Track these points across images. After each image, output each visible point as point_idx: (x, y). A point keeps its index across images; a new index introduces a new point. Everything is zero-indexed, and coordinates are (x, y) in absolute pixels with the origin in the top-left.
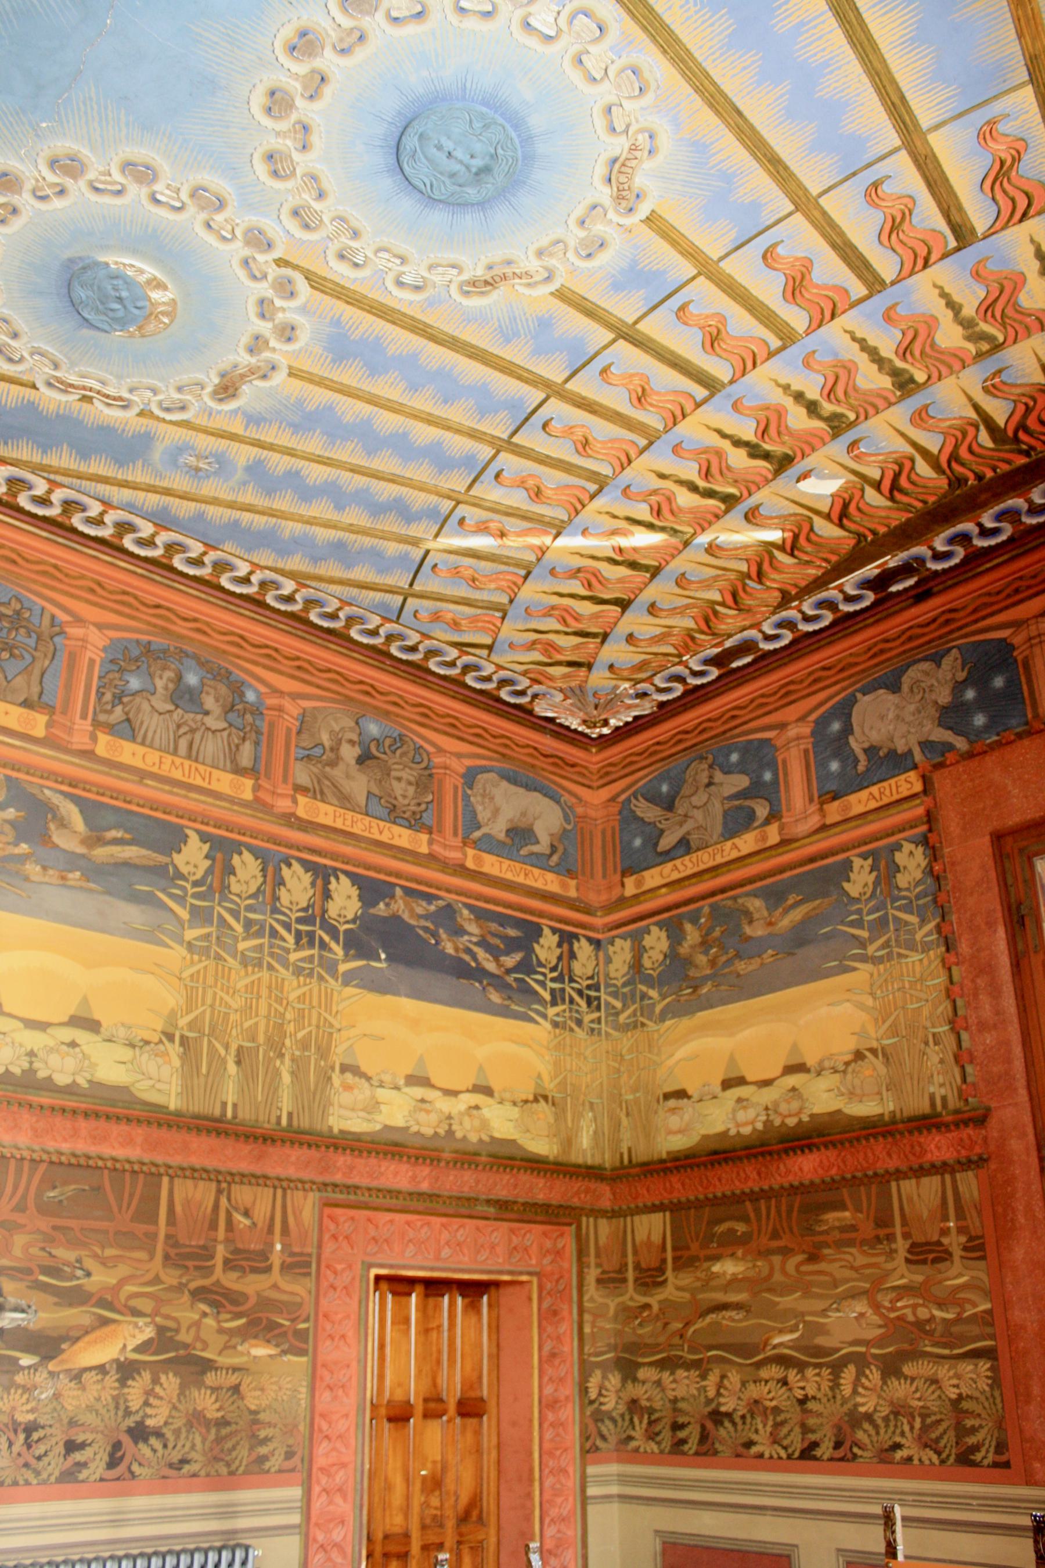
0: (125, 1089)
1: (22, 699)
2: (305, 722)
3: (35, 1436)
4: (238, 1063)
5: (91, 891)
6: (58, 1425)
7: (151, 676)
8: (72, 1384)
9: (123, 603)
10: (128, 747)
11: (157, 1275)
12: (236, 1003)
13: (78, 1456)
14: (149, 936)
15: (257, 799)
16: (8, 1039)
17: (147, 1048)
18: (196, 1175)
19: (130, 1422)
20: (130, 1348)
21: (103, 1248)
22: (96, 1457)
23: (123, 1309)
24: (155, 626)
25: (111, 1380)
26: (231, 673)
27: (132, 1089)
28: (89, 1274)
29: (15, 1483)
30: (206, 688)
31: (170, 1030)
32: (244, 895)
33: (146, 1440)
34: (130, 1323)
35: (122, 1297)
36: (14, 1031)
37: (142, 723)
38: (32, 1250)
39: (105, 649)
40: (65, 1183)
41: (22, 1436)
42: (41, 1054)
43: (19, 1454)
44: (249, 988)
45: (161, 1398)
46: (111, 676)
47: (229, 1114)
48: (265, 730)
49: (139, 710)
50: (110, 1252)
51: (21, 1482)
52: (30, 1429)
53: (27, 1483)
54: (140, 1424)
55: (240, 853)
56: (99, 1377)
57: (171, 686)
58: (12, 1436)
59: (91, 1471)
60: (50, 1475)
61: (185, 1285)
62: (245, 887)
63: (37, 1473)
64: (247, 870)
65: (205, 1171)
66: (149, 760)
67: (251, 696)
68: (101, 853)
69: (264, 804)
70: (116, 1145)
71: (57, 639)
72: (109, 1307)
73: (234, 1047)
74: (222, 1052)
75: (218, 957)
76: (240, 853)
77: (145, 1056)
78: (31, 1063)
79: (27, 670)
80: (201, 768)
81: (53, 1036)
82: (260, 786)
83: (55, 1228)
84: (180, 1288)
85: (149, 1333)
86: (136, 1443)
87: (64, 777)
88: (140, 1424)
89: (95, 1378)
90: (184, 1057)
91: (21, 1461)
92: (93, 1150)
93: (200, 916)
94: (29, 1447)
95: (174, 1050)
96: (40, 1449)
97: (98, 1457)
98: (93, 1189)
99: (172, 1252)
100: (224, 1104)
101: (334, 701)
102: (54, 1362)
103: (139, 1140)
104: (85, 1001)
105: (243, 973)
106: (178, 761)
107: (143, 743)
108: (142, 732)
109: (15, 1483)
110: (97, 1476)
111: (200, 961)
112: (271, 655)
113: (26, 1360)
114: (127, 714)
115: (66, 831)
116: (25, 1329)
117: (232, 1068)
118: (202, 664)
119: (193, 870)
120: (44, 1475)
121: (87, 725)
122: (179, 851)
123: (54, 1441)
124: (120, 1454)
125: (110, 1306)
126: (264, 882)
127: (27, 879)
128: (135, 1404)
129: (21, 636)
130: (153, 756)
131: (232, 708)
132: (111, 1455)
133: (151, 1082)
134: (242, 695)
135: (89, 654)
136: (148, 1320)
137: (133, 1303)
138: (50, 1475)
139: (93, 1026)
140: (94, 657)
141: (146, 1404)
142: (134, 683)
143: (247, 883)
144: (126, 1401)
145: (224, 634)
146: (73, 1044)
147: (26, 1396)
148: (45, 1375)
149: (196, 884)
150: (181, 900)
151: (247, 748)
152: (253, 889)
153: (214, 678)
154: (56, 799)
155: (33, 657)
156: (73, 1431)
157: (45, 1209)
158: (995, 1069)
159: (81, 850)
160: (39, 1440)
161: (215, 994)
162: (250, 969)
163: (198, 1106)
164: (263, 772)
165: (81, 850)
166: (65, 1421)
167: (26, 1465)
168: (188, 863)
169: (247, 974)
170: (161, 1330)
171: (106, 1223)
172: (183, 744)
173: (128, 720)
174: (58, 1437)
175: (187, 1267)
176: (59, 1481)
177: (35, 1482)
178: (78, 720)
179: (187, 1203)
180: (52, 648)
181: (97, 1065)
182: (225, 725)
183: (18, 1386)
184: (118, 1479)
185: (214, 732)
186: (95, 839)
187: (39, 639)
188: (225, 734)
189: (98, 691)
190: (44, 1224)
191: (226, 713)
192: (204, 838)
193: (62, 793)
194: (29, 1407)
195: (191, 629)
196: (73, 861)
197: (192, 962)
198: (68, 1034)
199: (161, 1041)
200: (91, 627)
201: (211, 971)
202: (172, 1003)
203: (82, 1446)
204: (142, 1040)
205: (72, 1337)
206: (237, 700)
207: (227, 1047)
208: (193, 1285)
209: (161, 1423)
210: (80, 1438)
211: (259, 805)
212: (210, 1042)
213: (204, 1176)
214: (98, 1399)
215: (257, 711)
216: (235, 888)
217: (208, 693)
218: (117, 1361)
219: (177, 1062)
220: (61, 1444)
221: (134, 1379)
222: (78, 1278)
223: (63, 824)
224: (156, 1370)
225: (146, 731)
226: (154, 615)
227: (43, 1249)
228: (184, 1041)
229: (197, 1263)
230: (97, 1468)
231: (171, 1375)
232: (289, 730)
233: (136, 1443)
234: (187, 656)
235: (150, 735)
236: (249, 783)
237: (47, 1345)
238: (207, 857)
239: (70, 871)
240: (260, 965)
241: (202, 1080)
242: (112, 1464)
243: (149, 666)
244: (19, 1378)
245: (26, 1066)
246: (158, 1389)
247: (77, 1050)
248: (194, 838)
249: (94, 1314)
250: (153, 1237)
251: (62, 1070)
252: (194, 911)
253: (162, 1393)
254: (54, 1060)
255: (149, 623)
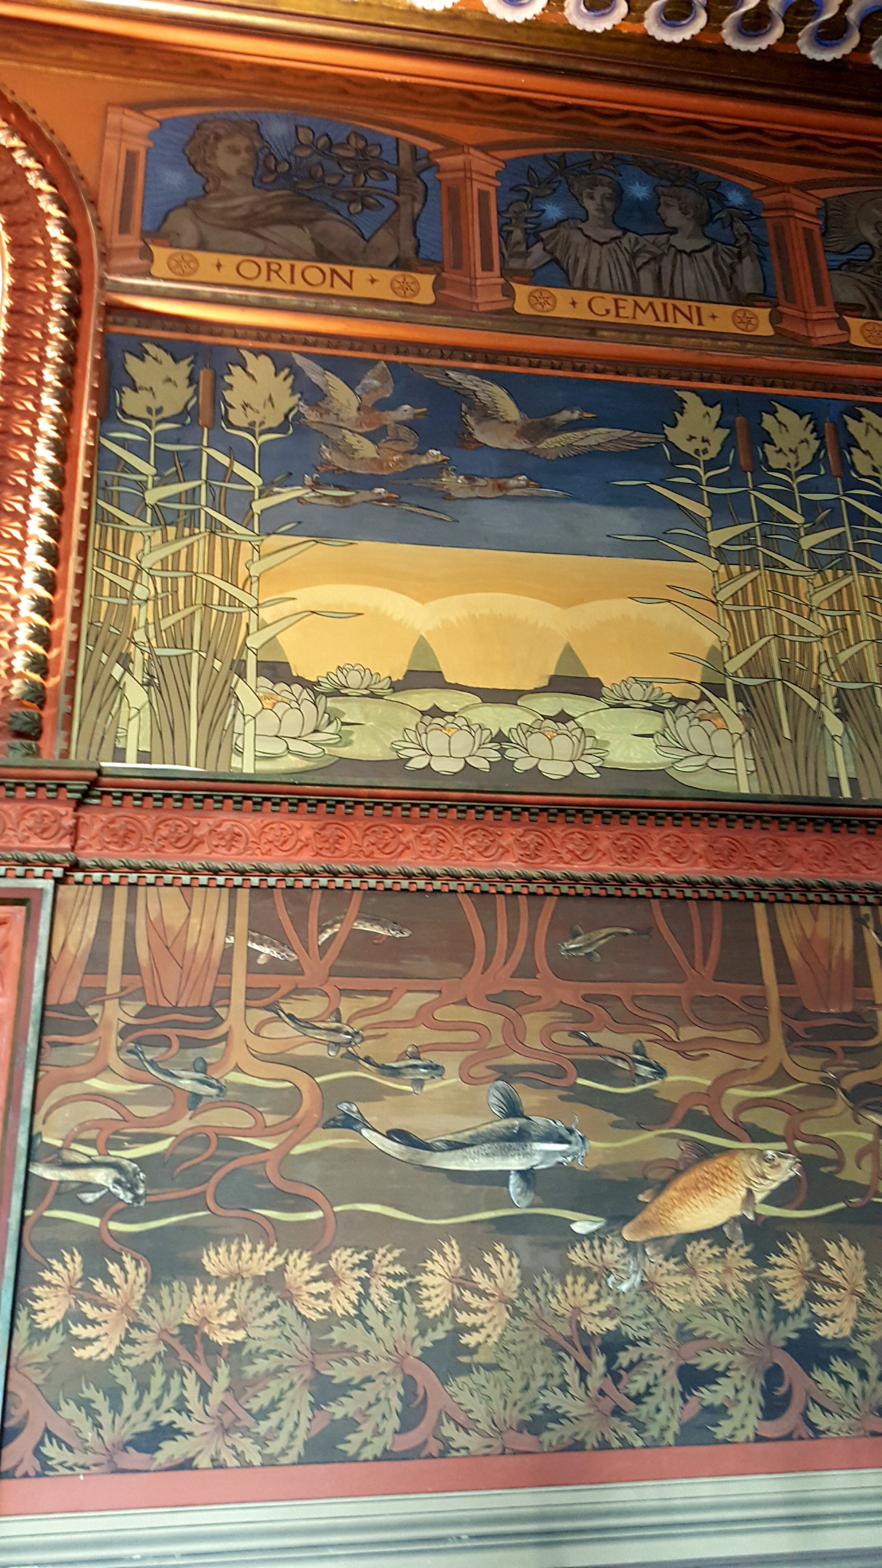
0: (661, 774)
1: (391, 258)
2: (831, 218)
3: (624, 1359)
4: (843, 716)
5: (547, 498)
6: (658, 1338)
7: (577, 198)
8: (670, 1265)
9: (511, 113)
10: (562, 295)
11: (781, 1068)
12: (819, 625)
13: (708, 1396)
14: (653, 548)
15: (779, 332)
16: (461, 722)
17: (684, 709)
18: (811, 896)
19: (789, 1330)
20: (759, 1197)
21: (676, 1027)
22: (738, 1397)
23: (733, 1129)
24: (566, 133)
25: (738, 1254)
26: (697, 173)
27: (671, 772)
28: (661, 1072)
29: (604, 1446)
30: (662, 199)
31: (717, 679)
32: (793, 470)
33: (825, 1366)
34: (750, 1152)
35: (728, 1109)
36: (466, 708)
37: (577, 261)
38: (555, 1037)
39: (498, 175)
40: (592, 926)
41: (600, 1360)
42: (515, 737)
43: (602, 1392)
44: (835, 601)
45: (836, 1286)
46: (515, 208)
47: (847, 793)
48: (771, 238)
49: (568, 245)
50: (688, 1033)
51: (616, 1444)
52: (613, 1344)
53: (626, 1445)
54: (808, 1335)
55: (773, 412)
56: (716, 1250)
57: (609, 205)
58: (583, 1359)
59: (736, 1422)
60: (663, 1430)
61: (836, 1082)
62: (792, 458)
63: (640, 1427)
64: (790, 436)
65: (829, 888)
66: (598, 306)
67: (735, 198)
68: (551, 444)
69: (795, 338)
70: (664, 859)
71: (425, 176)
72: (708, 1132)
73: (830, 692)
74: (813, 703)
75: (771, 564)
76: (773, 412)
77: (683, 723)
78: (502, 751)
79: (390, 222)
80: (683, 305)
81: (530, 710)
82: (781, 314)
83: (586, 998)
84: (826, 1089)
85: (787, 1170)
86: (808, 1370)
87: (470, 350)
88: (808, 1335)
89: (709, 1253)
90: (748, 717)
91: (607, 1405)
92: (626, 871)
93: (726, 510)
94: (616, 1378)
95: (729, 709)
96: (638, 1383)
97: (743, 1396)
98: (638, 932)
99: (798, 1027)
100: (835, 781)
101: (866, 182)
102: (630, 1225)
103: (699, 847)
104: (568, 652)
105: (818, 581)
106: (644, 302)
107: (584, 288)
108: (580, 272)
109: (604, 1446)
110: (749, 1432)
111: (743, 573)
112: (753, 140)
113: (583, 1225)
114: (551, 252)
115: (494, 423)
116: (571, 1170)
117: (834, 725)
118: (648, 169)
119: (701, 446)
120: (654, 1431)
121: (494, 277)
122: (674, 425)
123: (657, 1367)
124: (782, 1390)
125: (710, 1126)
126: (822, 446)
127: (447, 496)
128: (792, 1299)
129: (374, 181)
130: (604, 303)
131: (711, 216)
132: (767, 1392)
133: (702, 760)
134: (722, 198)
135: (476, 186)
136: (783, 1146)
137: (747, 1117)
138: (663, 1430)
139: (590, 688)
140: (485, 188)
141: (811, 1297)
142: (553, 212)
143: (794, 452)
144: (774, 1292)
145: (675, 124)
146: (563, 718)
147: (594, 1287)
148: (620, 1250)
149: (710, 465)
150: (692, 491)
151: (748, 269)
152: (806, 459)
153: (673, 184)
154: (469, 382)
155: (397, 203)
156: (689, 1349)
157: (565, 970)
158: (624, 1287)
159: (521, 445)
160: (632, 1365)
161: (779, 617)
162: (829, 573)
163: (789, 784)
164: (781, 295)
165: (521, 445)
166: (672, 1331)
167: (618, 1412)
168: (692, 438)
169: (826, 582)
170: (807, 1162)
171: (674, 985)
172: (646, 278)
173: (555, 260)
174: (663, 1361)
175: (831, 1051)
176: (681, 1440)
177: (639, 1443)
178: (479, 273)
179: (806, 944)
180: (421, 187)
181: (607, 743)
182: (706, 242)
183: (577, 1270)
184: (788, 1437)
185: (689, 254)
186: (538, 427)
187: (398, 179)
188: (708, 254)
189: (500, 230)
190: (570, 993)
191: (703, 226)
192: (709, 398)
193: (476, 372)
194: (602, 1307)
195: (621, 128)
196: (510, 463)
197: (730, 577)
198: (550, 704)
199: (704, 698)
200: (472, 151)
201: (764, 584)
202: (709, 639)
203: (711, 1376)
204: (672, 699)
205: (660, 1179)
206: (716, 207)
207: (817, 694)
208: (849, 1082)
209: (847, 1332)
210: (705, 1362)
211: (784, 340)
212: (785, 688)
213: (826, 897)
214: (722, 1291)
215: (750, 215)
216: (776, 461)
217: (667, 205)
218: (741, 1220)
219: (737, 726)
220: (672, 1372)
221: (779, 1253)
222: (645, 1080)
223: (487, 414)
224: (817, 1233)
225: (586, 270)
226: (560, 120)
227: (575, 1034)
228: (741, 692)
229: (846, 1043)
230: (745, 1418)
231: (844, 1243)
232: (808, 233)
233: (808, 1370)
234: (627, 163)
235: (592, 273)
236: (763, 314)
237: (618, 1197)
238: (719, 425)
239: (511, 477)
240: (847, 568)
241: (787, 747)
242: (773, 1408)
243: (570, 186)
244: (577, 1256)
245: (495, 756)
246: (827, 1270)
247: (571, 725)
248: (693, 403)
249: (684, 1139)
250: (758, 1003)
251: (553, 759)
252: (715, 502)
253: (836, 1277)
254: (537, 743)
255: (557, 131)
